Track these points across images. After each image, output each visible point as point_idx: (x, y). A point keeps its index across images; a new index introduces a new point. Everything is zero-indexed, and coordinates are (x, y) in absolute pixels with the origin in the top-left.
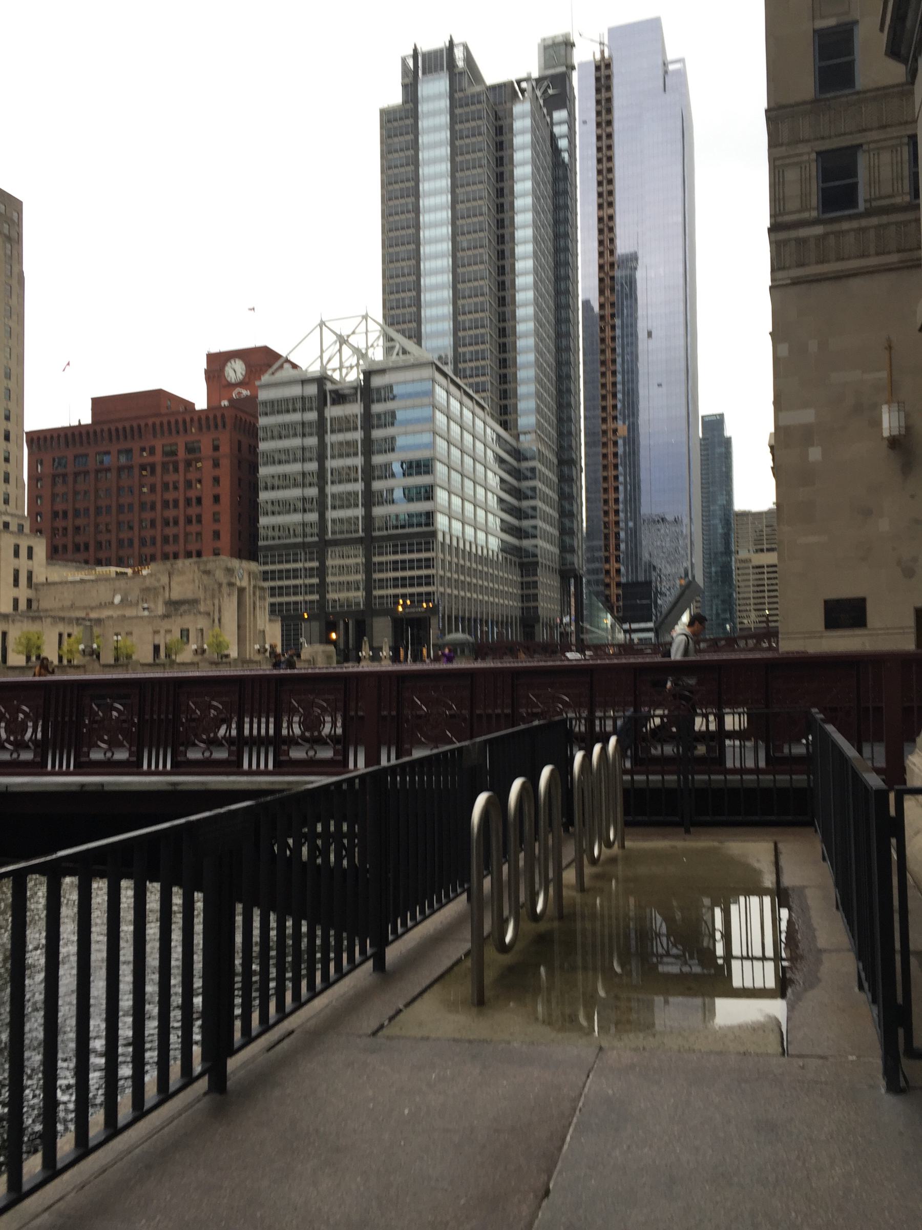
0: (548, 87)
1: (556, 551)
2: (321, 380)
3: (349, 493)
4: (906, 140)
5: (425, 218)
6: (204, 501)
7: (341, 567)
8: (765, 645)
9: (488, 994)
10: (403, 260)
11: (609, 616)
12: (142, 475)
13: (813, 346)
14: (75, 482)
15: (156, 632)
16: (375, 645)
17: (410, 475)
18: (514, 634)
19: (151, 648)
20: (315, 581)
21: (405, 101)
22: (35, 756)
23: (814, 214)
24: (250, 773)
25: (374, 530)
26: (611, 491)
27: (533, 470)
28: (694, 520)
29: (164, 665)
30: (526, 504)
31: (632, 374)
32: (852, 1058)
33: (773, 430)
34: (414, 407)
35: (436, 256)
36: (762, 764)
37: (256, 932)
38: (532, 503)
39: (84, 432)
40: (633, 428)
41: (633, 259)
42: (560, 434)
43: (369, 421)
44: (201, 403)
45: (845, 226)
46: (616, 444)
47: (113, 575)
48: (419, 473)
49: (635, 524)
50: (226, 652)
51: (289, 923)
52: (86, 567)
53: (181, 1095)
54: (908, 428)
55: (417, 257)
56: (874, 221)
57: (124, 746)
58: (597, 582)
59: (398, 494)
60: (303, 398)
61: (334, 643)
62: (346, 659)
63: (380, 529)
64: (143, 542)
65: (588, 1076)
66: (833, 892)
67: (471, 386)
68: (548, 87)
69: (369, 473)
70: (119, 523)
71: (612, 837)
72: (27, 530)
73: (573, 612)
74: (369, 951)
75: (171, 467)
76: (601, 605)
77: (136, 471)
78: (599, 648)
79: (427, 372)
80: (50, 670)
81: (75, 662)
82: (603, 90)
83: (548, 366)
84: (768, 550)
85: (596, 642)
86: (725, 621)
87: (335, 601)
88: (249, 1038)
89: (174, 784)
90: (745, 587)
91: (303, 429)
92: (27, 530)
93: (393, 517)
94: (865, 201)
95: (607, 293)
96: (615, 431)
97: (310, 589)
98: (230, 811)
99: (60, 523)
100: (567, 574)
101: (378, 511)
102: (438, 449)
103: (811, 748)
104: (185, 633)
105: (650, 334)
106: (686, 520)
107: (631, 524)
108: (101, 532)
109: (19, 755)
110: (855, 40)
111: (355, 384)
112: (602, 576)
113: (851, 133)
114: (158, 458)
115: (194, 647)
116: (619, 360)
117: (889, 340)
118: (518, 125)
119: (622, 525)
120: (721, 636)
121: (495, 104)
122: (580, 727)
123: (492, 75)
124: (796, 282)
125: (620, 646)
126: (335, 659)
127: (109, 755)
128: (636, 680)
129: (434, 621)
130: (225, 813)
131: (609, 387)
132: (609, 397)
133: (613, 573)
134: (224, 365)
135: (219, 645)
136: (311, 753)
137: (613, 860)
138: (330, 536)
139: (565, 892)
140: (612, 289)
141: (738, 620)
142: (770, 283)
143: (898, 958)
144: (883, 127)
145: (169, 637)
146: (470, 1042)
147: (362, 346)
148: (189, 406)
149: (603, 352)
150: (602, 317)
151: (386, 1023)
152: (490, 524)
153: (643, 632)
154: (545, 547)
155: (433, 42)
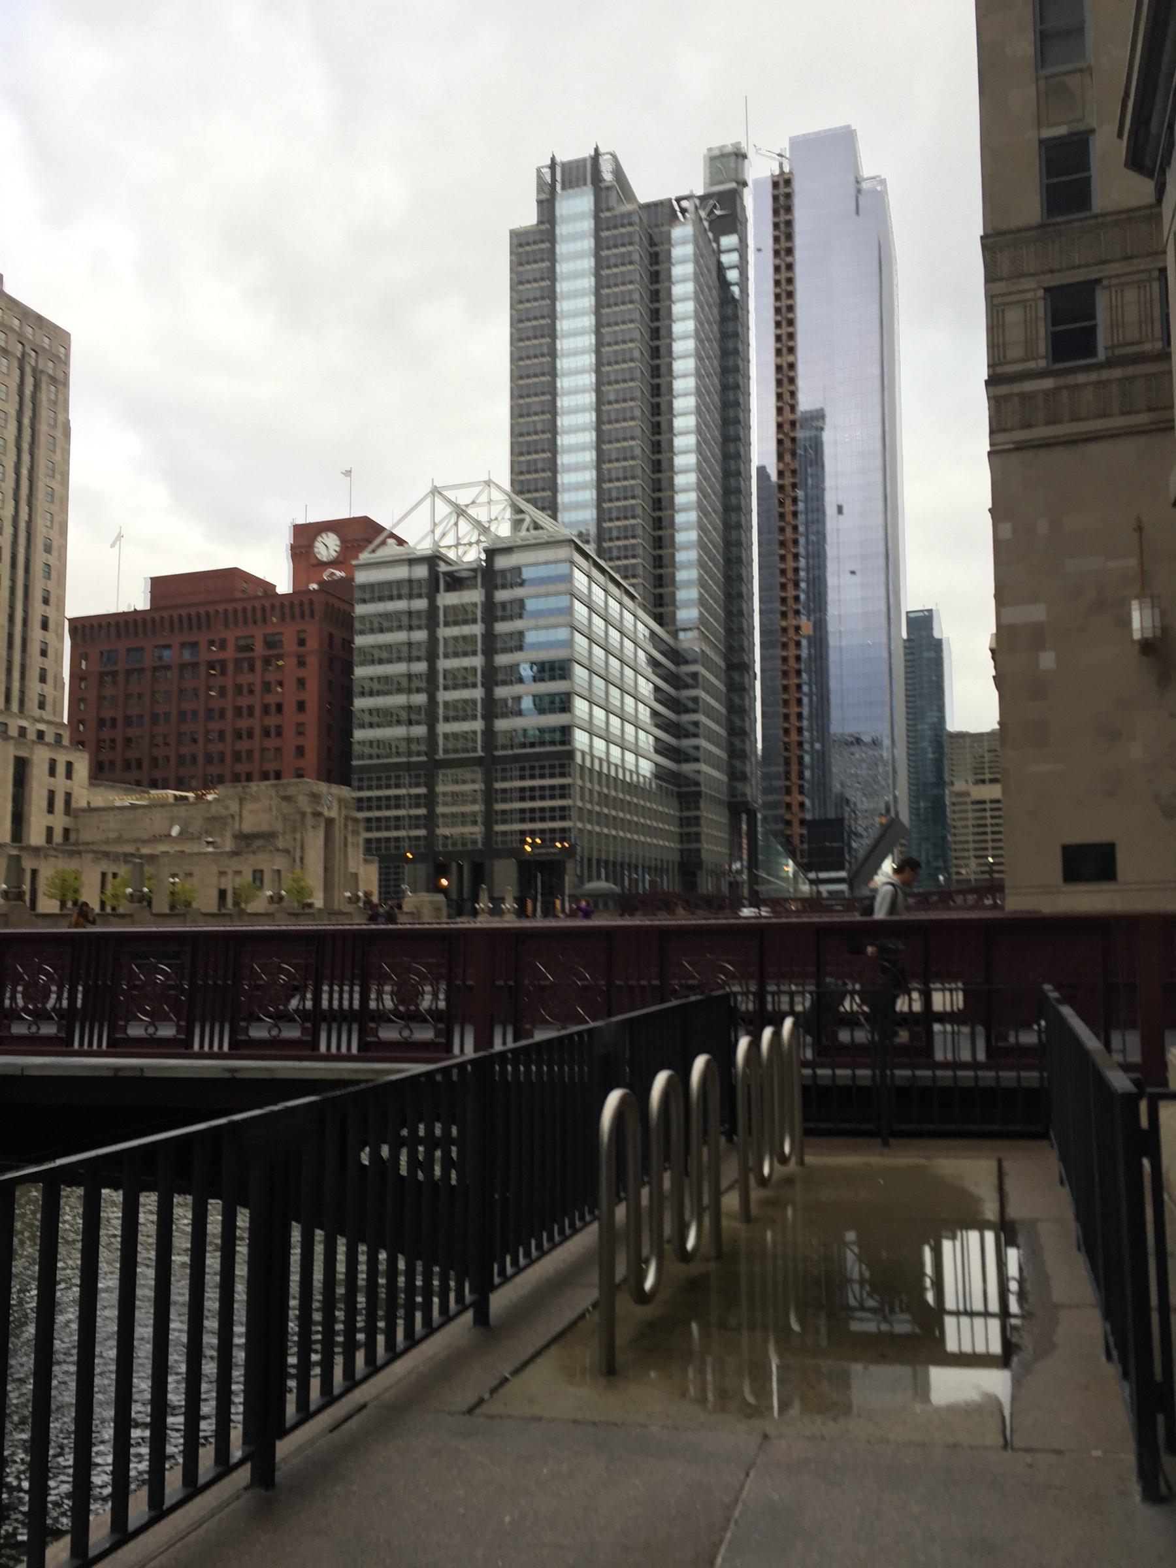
0: (715, 207)
1: (724, 778)
2: (433, 560)
3: (465, 701)
4: (1156, 274)
5: (563, 364)
6: (285, 708)
7: (455, 795)
8: (988, 902)
9: (620, 1359)
10: (536, 414)
11: (791, 862)
12: (220, 674)
13: (1043, 526)
14: (127, 681)
15: (222, 874)
16: (496, 895)
17: (542, 680)
18: (669, 884)
19: (215, 894)
20: (422, 811)
21: (540, 222)
22: (59, 1031)
23: (1042, 363)
24: (328, 1058)
25: (496, 749)
26: (793, 703)
27: (695, 675)
28: (897, 744)
29: (230, 915)
30: (686, 718)
31: (818, 557)
32: (1097, 1453)
33: (994, 630)
34: (547, 595)
35: (576, 411)
36: (981, 1056)
37: (341, 1268)
38: (694, 717)
39: (139, 619)
40: (820, 626)
41: (818, 417)
42: (729, 631)
43: (491, 612)
44: (284, 585)
45: (1081, 378)
46: (798, 644)
47: (171, 800)
48: (553, 678)
49: (823, 746)
50: (309, 901)
51: (383, 1256)
52: (138, 788)
53: (216, 1489)
54: (1165, 629)
55: (552, 410)
56: (1118, 373)
57: (171, 1020)
58: (777, 819)
59: (527, 703)
60: (410, 581)
61: (444, 891)
62: (460, 913)
63: (504, 747)
64: (209, 759)
65: (747, 1475)
66: (1073, 1229)
67: (617, 569)
68: (715, 207)
69: (492, 677)
70: (180, 735)
71: (787, 1149)
72: (66, 741)
73: (745, 857)
74: (468, 1297)
75: (245, 665)
76: (780, 848)
77: (203, 669)
78: (777, 903)
79: (564, 552)
80: (91, 919)
81: (121, 910)
82: (782, 212)
83: (714, 546)
84: (993, 781)
85: (774, 895)
86: (938, 870)
87: (446, 837)
88: (306, 1414)
89: (233, 1070)
90: (962, 828)
91: (409, 620)
92: (66, 741)
93: (521, 732)
94: (1106, 348)
95: (788, 458)
96: (798, 629)
97: (415, 822)
98: (287, 1109)
99: (106, 734)
100: (737, 808)
101: (501, 724)
102: (577, 648)
103: (1043, 1036)
104: (258, 875)
105: (840, 510)
106: (887, 742)
107: (818, 746)
108: (157, 745)
109: (39, 1028)
110: (1091, 153)
111: (474, 566)
112: (782, 811)
113: (1087, 266)
114: (230, 654)
115: (270, 893)
116: (802, 540)
117: (1139, 519)
118: (677, 252)
119: (807, 746)
120: (933, 889)
121: (650, 227)
122: (747, 1005)
123: (646, 190)
124: (1020, 447)
125: (804, 901)
126: (445, 912)
127: (151, 1030)
128: (824, 945)
129: (570, 866)
130: (279, 1111)
131: (790, 574)
132: (790, 586)
133: (795, 808)
134: (314, 539)
135: (301, 892)
136: (406, 1033)
137: (789, 1181)
138: (441, 755)
139: (725, 1222)
140: (794, 454)
141: (954, 869)
142: (988, 449)
143: (1155, 1317)
144: (1127, 258)
145: (238, 880)
146: (594, 1424)
147: (483, 518)
148: (269, 588)
149: (782, 530)
150: (781, 488)
151: (487, 1396)
152: (641, 744)
153: (833, 881)
154: (710, 774)
155: (574, 151)
